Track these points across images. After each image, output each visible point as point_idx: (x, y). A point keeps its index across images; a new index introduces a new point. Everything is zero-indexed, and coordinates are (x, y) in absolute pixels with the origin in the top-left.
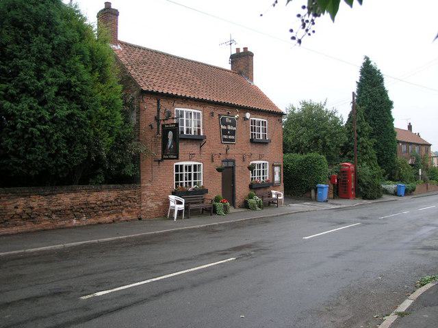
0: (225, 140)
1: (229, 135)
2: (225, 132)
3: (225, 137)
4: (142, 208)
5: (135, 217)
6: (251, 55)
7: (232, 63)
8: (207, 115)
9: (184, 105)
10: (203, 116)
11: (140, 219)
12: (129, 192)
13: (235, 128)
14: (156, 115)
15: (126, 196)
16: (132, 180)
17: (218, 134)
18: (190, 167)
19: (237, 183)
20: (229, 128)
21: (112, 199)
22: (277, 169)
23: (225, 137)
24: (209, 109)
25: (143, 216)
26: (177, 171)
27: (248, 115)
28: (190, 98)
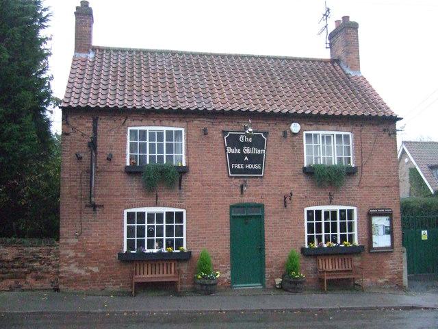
0: (234, 171)
1: (247, 162)
2: (234, 158)
3: (237, 166)
4: (61, 275)
5: (48, 285)
6: (355, 26)
7: (331, 46)
8: (196, 133)
9: (145, 122)
10: (187, 135)
11: (57, 290)
12: (38, 249)
13: (263, 151)
14: (91, 135)
15: (33, 254)
16: (50, 231)
17: (222, 160)
18: (334, 213)
19: (381, 246)
20: (247, 150)
21: (9, 258)
22: (380, 222)
23: (237, 166)
24: (205, 123)
25: (61, 287)
26: (310, 218)
27: (295, 127)
28: (134, 110)
